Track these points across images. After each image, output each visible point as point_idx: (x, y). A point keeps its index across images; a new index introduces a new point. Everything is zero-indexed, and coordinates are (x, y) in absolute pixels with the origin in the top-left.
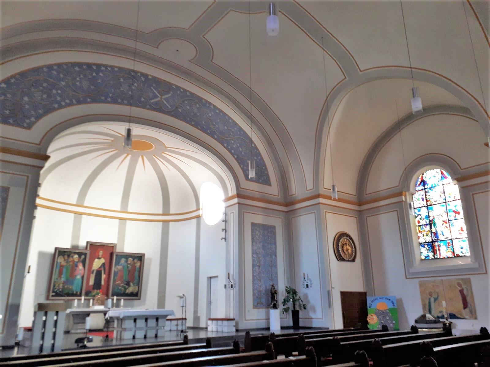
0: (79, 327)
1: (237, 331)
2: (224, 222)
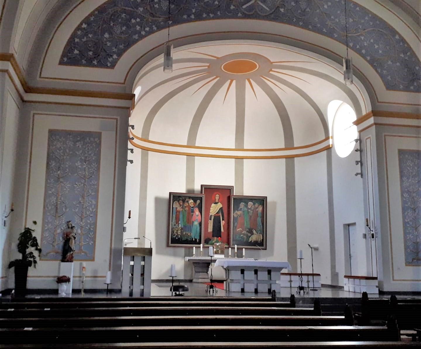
0: (200, 277)
1: (381, 293)
2: (359, 152)
